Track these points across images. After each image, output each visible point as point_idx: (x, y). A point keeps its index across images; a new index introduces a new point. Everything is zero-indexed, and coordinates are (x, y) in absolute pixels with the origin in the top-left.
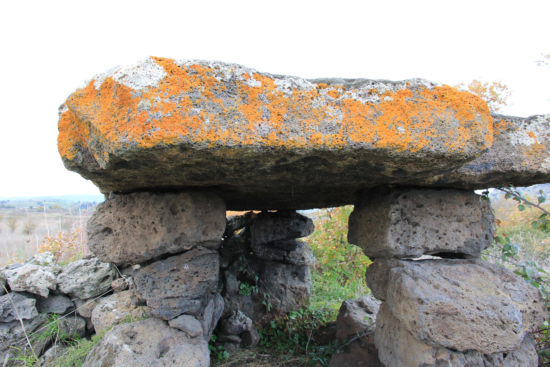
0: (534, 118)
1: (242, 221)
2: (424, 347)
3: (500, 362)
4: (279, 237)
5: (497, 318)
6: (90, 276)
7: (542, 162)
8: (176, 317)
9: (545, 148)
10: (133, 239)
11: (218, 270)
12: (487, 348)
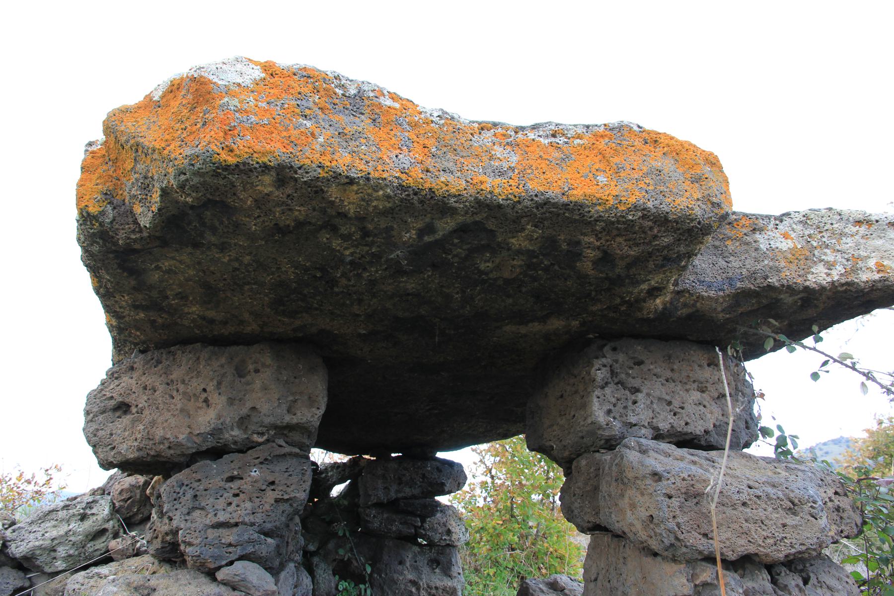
0: (787, 214)
1: (344, 470)
2: (669, 568)
3: (800, 590)
4: (408, 492)
5: (781, 496)
6: (71, 527)
7: (809, 273)
8: (231, 563)
9: (808, 254)
10: (168, 415)
11: (309, 483)
12: (774, 547)
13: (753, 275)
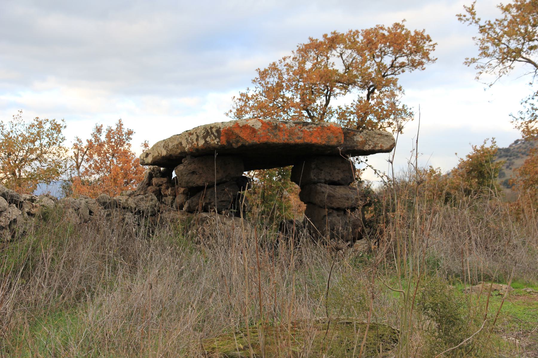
13: (351, 146)
